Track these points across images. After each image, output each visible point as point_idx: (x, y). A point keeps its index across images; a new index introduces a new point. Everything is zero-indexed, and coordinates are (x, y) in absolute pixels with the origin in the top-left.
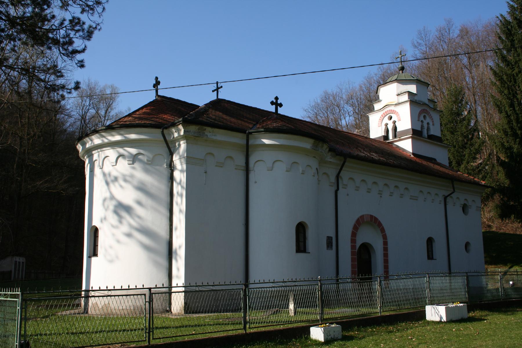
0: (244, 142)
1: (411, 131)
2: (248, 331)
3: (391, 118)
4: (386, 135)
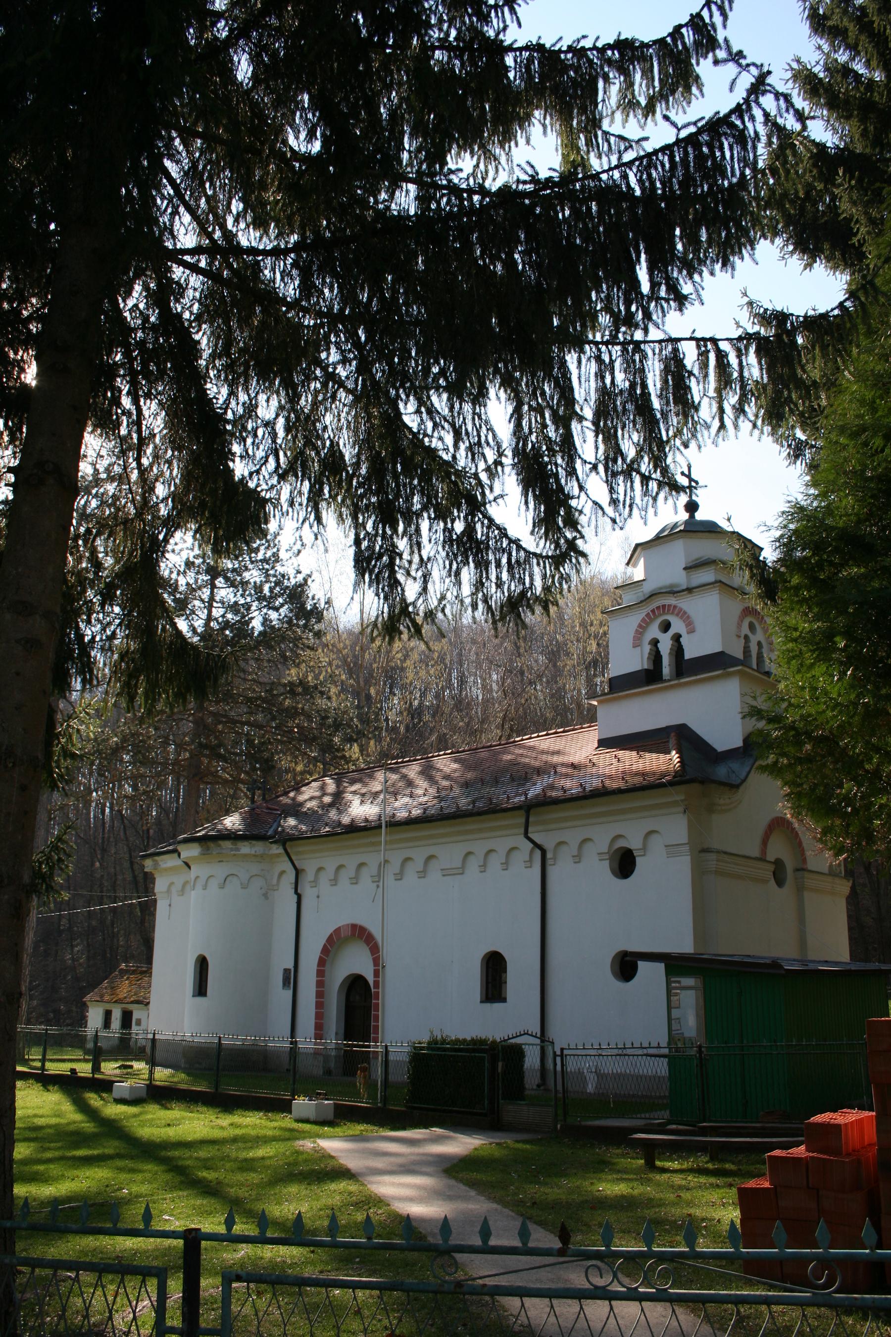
3: (666, 627)
4: (651, 668)
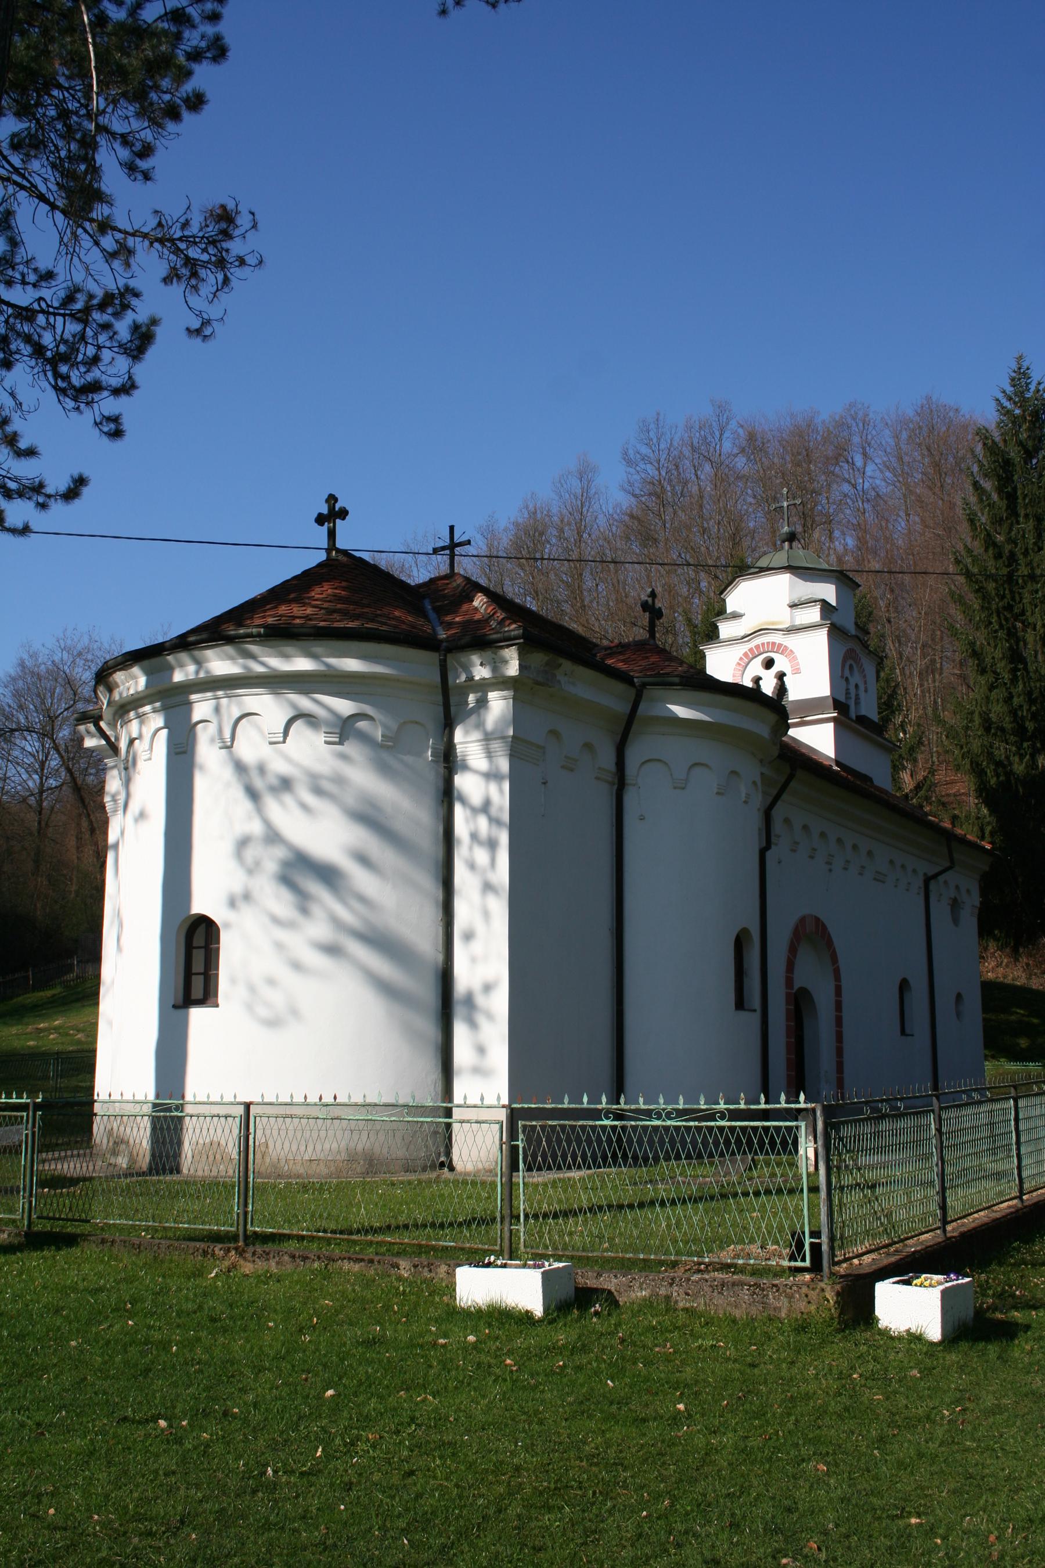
0: (622, 708)
3: (769, 664)
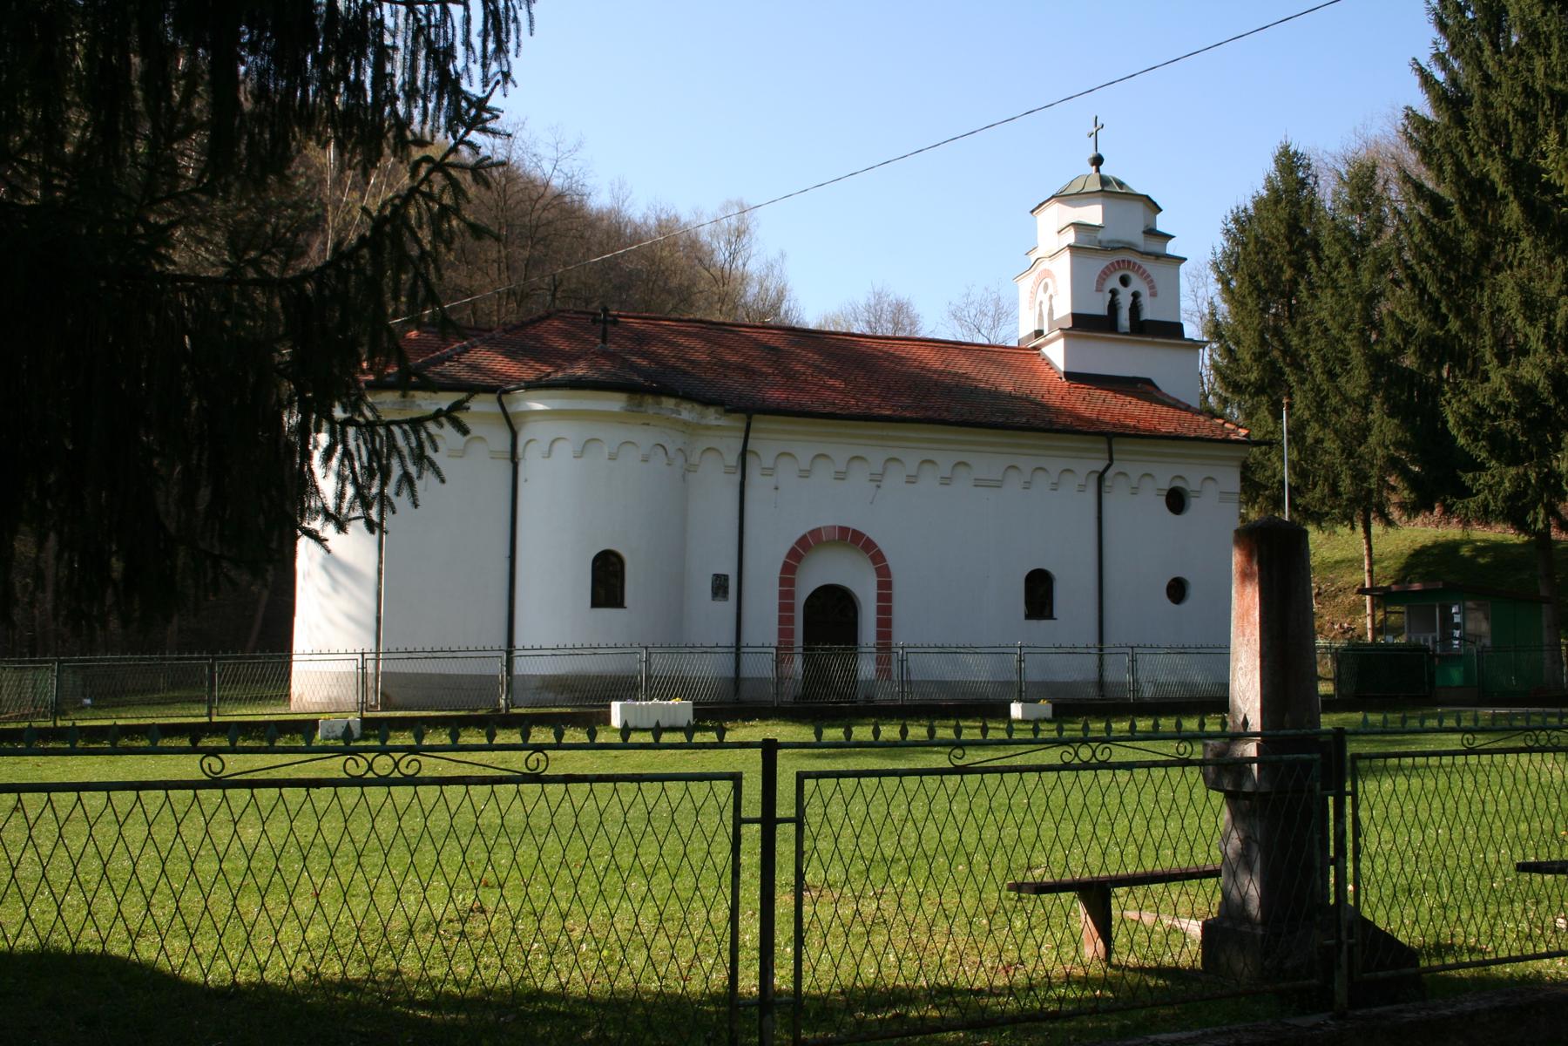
1: (1070, 317)
2: (215, 719)
3: (1125, 281)
